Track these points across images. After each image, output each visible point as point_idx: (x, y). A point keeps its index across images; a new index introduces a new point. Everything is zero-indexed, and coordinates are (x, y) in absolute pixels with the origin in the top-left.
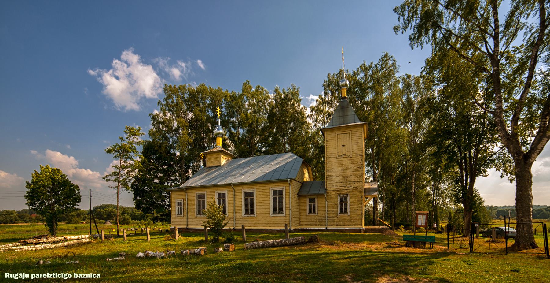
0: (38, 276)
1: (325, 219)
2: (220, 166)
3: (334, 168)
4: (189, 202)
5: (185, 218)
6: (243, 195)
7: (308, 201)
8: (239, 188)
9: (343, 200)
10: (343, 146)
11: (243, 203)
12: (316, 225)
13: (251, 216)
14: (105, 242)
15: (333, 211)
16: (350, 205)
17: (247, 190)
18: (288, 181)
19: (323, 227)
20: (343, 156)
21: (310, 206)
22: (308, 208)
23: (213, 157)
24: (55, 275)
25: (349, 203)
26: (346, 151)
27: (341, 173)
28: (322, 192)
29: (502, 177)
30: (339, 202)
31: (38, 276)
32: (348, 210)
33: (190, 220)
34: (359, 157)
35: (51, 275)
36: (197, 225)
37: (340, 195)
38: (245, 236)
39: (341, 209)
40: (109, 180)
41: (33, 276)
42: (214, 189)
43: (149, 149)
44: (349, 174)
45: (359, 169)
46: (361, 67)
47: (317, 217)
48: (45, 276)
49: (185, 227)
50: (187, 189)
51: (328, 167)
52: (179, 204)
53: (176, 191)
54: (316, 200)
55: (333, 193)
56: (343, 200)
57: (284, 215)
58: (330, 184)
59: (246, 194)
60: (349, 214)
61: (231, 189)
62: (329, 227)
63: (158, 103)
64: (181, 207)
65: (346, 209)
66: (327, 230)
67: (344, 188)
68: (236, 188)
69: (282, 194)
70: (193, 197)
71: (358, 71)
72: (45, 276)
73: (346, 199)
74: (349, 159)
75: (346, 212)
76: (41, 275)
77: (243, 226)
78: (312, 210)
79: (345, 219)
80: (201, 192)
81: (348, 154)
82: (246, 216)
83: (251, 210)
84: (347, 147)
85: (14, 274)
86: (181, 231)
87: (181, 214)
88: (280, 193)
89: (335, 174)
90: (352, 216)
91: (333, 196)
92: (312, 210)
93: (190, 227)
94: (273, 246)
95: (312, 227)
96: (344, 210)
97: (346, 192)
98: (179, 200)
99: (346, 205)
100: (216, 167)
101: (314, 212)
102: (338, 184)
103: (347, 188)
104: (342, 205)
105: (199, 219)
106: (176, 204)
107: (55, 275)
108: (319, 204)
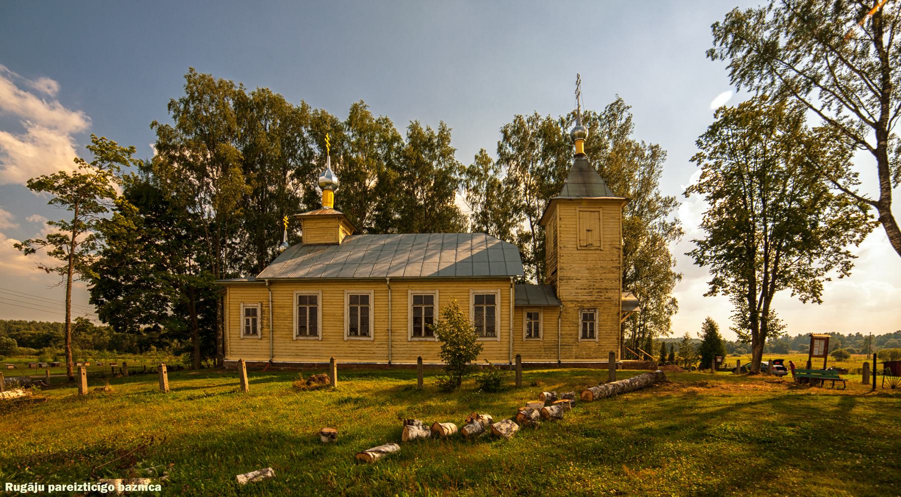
0: (59, 488)
1: (555, 348)
2: (338, 244)
3: (574, 265)
4: (277, 310)
5: (265, 341)
6: (410, 300)
7: (525, 315)
8: (402, 287)
9: (588, 318)
10: (588, 231)
11: (410, 316)
12: (540, 357)
13: (428, 339)
14: (90, 396)
15: (571, 334)
16: (600, 326)
17: (419, 292)
18: (509, 279)
19: (554, 361)
20: (588, 247)
21: (529, 325)
22: (525, 328)
23: (320, 225)
24: (87, 487)
25: (597, 322)
26: (593, 239)
27: (586, 274)
28: (556, 303)
29: (793, 295)
30: (580, 321)
31: (59, 488)
32: (597, 333)
33: (280, 345)
34: (615, 251)
35: (81, 486)
36: (297, 355)
37: (582, 308)
38: (246, 380)
39: (585, 331)
40: (33, 251)
41: (51, 488)
42: (341, 287)
43: (138, 194)
44: (598, 276)
45: (615, 270)
46: (573, 113)
47: (541, 343)
48: (70, 488)
49: (386, 362)
50: (273, 282)
51: (562, 262)
52: (251, 312)
53: (242, 285)
54: (541, 316)
55: (570, 305)
56: (588, 318)
57: (499, 339)
58: (565, 291)
59: (417, 299)
60: (597, 340)
61: (383, 287)
62: (563, 361)
63: (170, 105)
64: (255, 321)
65: (592, 332)
66: (560, 365)
67: (589, 298)
68: (395, 287)
69: (494, 303)
70: (288, 302)
71: (568, 119)
72: (70, 488)
73: (592, 316)
74: (598, 252)
75: (592, 336)
76: (64, 486)
77: (420, 359)
78: (533, 332)
79: (590, 348)
80: (307, 291)
81: (596, 244)
82: (416, 339)
83: (310, 328)
84: (596, 233)
85: (62, 492)
86: (254, 369)
87: (255, 332)
88: (491, 299)
89: (573, 275)
90: (603, 343)
91: (570, 310)
92: (533, 332)
93: (277, 360)
94: (623, 391)
95: (534, 361)
96: (588, 334)
97: (592, 304)
98: (250, 306)
99: (592, 325)
100: (333, 244)
101: (537, 335)
102: (579, 291)
103: (594, 298)
104: (585, 325)
105: (301, 344)
106: (242, 312)
107: (87, 487)
108: (546, 323)
